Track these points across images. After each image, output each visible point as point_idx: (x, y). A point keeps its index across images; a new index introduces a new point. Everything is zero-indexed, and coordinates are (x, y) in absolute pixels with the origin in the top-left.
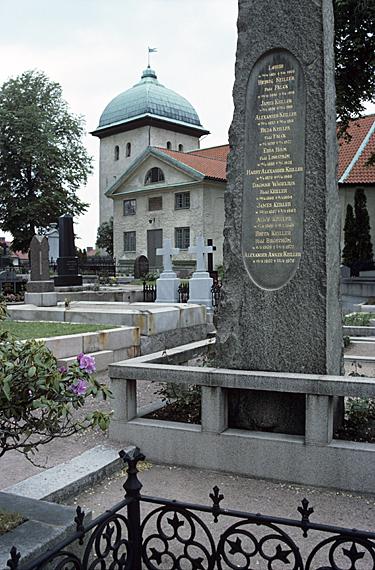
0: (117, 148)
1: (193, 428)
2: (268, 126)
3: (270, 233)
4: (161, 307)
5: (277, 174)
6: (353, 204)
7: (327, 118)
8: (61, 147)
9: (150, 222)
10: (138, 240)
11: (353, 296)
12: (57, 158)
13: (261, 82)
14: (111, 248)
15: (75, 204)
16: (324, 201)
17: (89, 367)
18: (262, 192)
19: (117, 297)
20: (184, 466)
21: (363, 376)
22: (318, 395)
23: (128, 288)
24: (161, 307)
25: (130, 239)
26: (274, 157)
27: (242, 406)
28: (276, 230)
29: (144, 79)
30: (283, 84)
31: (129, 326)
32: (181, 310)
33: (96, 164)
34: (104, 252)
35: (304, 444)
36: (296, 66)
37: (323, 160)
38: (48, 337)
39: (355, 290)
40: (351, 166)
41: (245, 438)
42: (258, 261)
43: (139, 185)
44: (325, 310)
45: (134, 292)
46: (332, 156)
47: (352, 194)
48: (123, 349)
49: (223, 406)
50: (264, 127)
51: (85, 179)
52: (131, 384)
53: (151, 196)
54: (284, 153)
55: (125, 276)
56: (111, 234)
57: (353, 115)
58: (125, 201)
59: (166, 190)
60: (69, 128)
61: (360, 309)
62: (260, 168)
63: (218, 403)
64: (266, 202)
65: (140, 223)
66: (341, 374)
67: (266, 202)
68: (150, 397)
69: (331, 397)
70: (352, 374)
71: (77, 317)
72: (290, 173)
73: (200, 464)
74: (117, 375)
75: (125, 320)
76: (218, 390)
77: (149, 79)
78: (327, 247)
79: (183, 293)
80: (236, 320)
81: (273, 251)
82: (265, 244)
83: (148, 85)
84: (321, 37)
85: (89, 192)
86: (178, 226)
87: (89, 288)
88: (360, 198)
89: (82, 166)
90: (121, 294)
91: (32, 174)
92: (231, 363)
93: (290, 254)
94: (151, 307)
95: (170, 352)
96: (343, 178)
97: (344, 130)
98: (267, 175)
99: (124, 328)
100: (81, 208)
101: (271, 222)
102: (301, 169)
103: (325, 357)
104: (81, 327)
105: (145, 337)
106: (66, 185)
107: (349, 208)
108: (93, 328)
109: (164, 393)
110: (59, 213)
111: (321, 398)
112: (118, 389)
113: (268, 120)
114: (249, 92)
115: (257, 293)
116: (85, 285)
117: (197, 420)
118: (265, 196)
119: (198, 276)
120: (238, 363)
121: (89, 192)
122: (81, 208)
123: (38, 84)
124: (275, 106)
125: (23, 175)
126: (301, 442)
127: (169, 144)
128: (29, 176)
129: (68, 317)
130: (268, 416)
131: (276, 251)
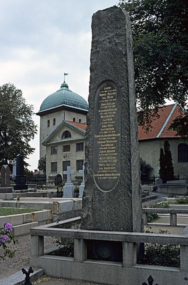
0: (49, 121)
1: (70, 259)
2: (104, 115)
3: (106, 164)
4: (64, 200)
5: (109, 137)
6: (163, 148)
7: (131, 111)
8: (21, 120)
9: (64, 157)
10: (58, 166)
11: (163, 193)
12: (20, 126)
13: (101, 95)
14: (45, 170)
15: (28, 149)
16: (130, 150)
17: (9, 229)
18: (102, 145)
19: (44, 195)
20: (66, 279)
21: (152, 233)
22: (128, 242)
23: (50, 191)
24: (64, 200)
25: (54, 166)
26: (107, 129)
27: (93, 248)
28: (108, 163)
29: (62, 88)
30: (111, 95)
31: (48, 209)
32: (74, 201)
33: (38, 129)
34: (42, 173)
35: (122, 266)
36: (116, 88)
37: (129, 130)
38: (6, 215)
39: (165, 190)
40: (162, 129)
41: (94, 264)
42: (100, 178)
43: (58, 139)
44: (132, 201)
45: (52, 192)
46: (134, 129)
47: (163, 142)
48: (44, 221)
49: (84, 249)
50: (102, 115)
51: (33, 136)
52: (41, 238)
53: (64, 145)
54: (111, 127)
55: (51, 185)
56: (45, 163)
57: (160, 105)
58: (52, 147)
59: (72, 142)
60: (27, 111)
61: (166, 200)
62: (101, 134)
63: (82, 246)
64: (104, 150)
65: (60, 157)
66: (141, 232)
67: (104, 150)
68: (51, 244)
69: (134, 243)
70: (147, 232)
71: (22, 205)
72: (114, 137)
73: (73, 277)
74: (33, 233)
75: (46, 206)
76: (82, 240)
77: (65, 88)
78: (132, 171)
79: (76, 193)
80: (90, 206)
81: (107, 173)
82: (104, 170)
83: (64, 91)
84: (127, 75)
85: (35, 143)
86: (78, 159)
87: (31, 191)
88: (167, 145)
89: (31, 130)
90: (46, 193)
91: (7, 134)
92: (88, 227)
93: (115, 175)
94: (60, 200)
95: (60, 222)
96: (158, 135)
97: (156, 113)
98: (104, 137)
99: (45, 211)
100: (31, 150)
101: (106, 159)
102: (119, 135)
103: (132, 224)
104: (23, 210)
105: (55, 213)
106: (23, 139)
107: (162, 150)
108: (29, 211)
109: (57, 242)
110: (21, 151)
111: (130, 244)
112: (32, 241)
113: (104, 112)
114: (95, 100)
115: (100, 193)
116: (29, 189)
117: (72, 256)
118: (103, 147)
119: (67, 185)
120: (91, 227)
121: (35, 143)
122: (31, 150)
123: (11, 89)
124: (107, 106)
125: (2, 134)
126: (121, 265)
127: (74, 119)
128: (5, 135)
129: (18, 205)
130: (106, 253)
131: (109, 173)
